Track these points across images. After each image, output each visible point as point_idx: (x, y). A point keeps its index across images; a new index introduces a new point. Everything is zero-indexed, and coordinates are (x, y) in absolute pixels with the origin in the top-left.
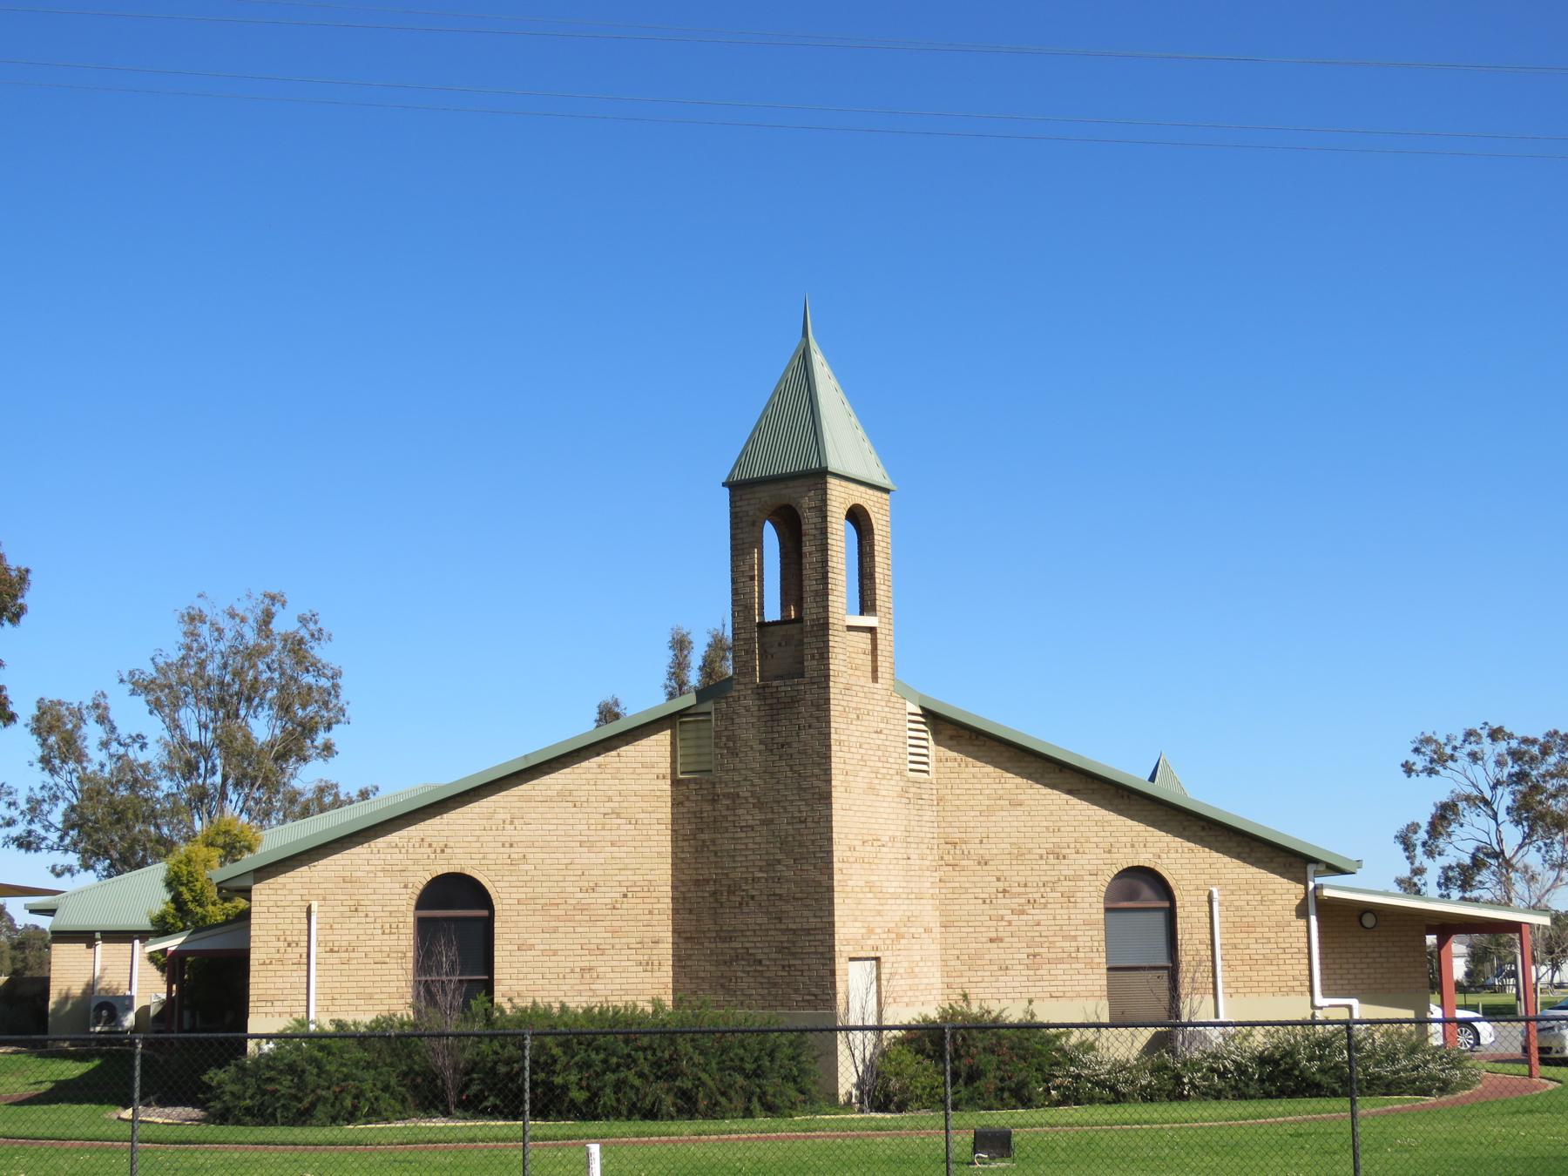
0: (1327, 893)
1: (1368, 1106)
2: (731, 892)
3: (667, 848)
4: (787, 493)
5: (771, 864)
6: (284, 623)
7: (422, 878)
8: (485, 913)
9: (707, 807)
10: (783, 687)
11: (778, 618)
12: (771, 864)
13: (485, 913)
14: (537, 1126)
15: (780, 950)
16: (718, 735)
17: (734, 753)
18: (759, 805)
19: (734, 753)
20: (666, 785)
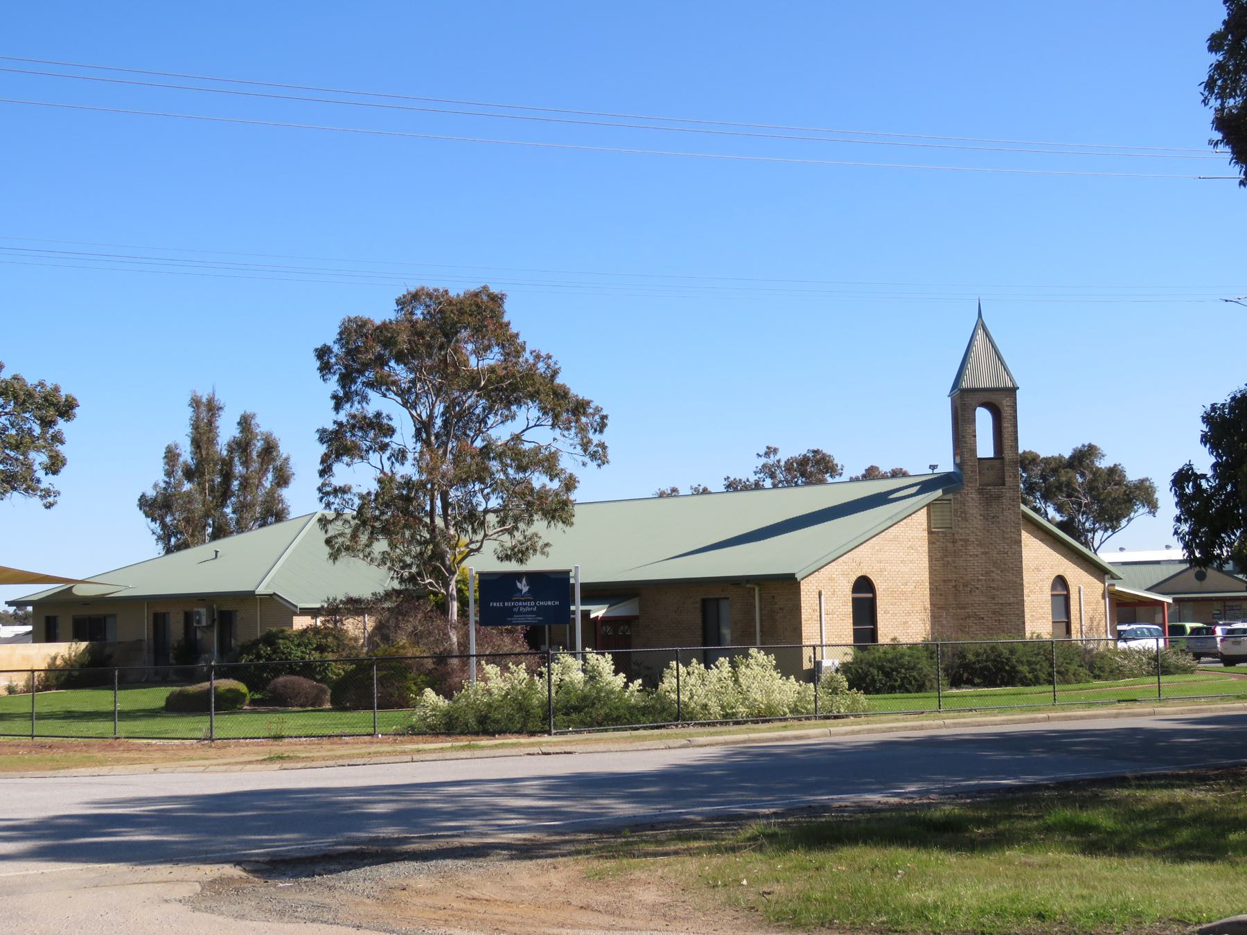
0: (1117, 588)
1: (28, 709)
2: (965, 586)
3: (926, 564)
4: (993, 398)
5: (988, 573)
6: (227, 431)
7: (854, 578)
8: (870, 595)
9: (950, 545)
10: (994, 490)
11: (992, 455)
12: (988, 573)
13: (870, 595)
14: (380, 714)
15: (994, 613)
16: (956, 510)
17: (966, 520)
18: (980, 545)
19: (966, 520)
20: (926, 534)
